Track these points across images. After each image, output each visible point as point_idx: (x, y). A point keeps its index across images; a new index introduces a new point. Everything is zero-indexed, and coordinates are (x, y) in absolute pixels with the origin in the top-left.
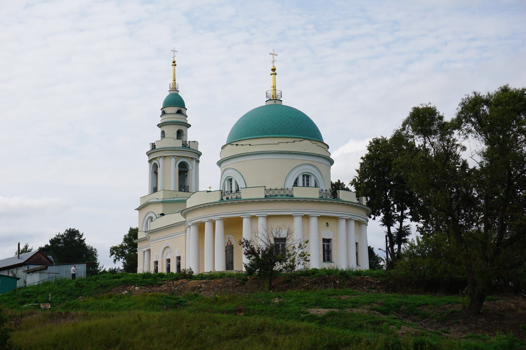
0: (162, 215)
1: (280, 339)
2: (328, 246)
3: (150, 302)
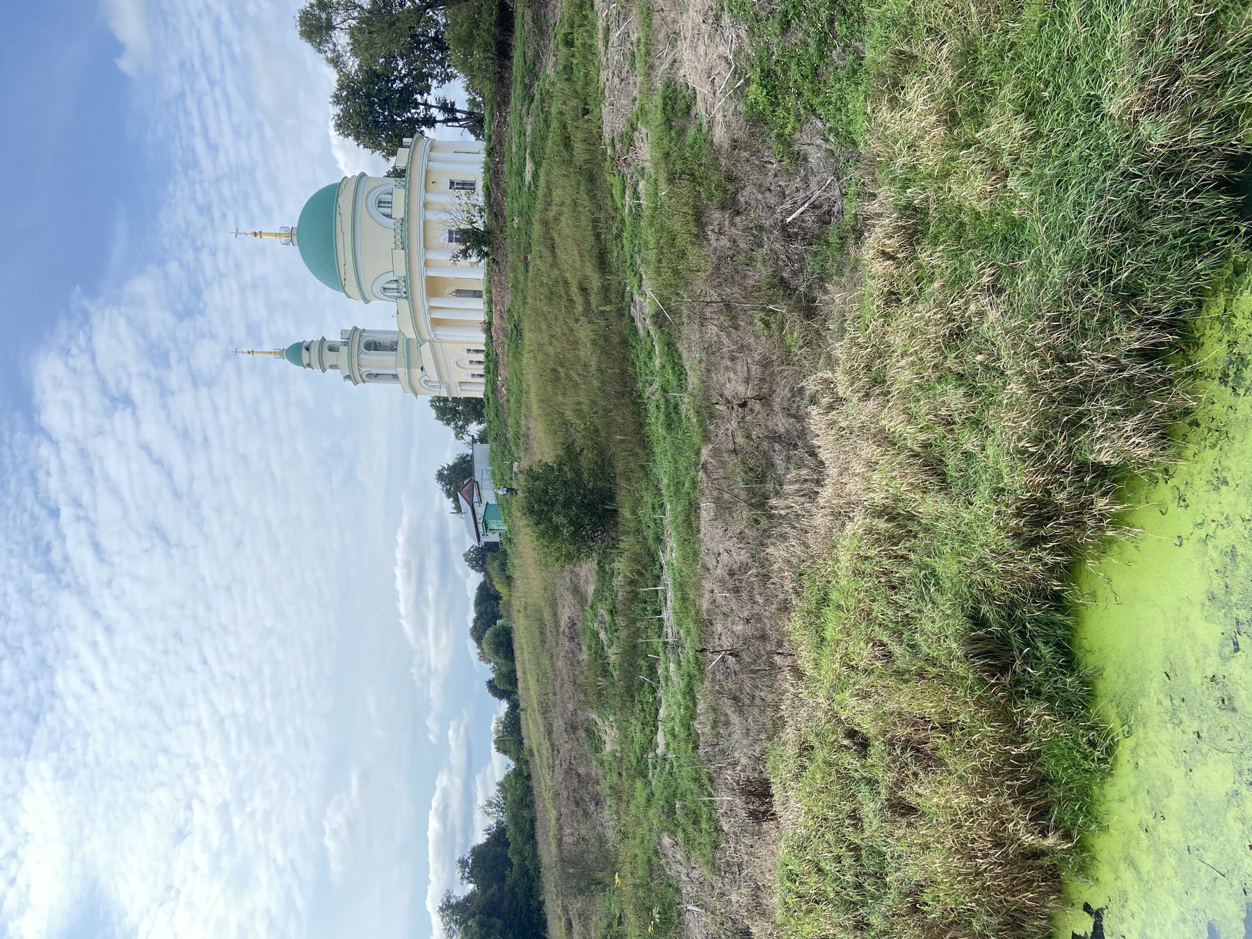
0: (422, 369)
1: (557, 200)
3: (514, 356)
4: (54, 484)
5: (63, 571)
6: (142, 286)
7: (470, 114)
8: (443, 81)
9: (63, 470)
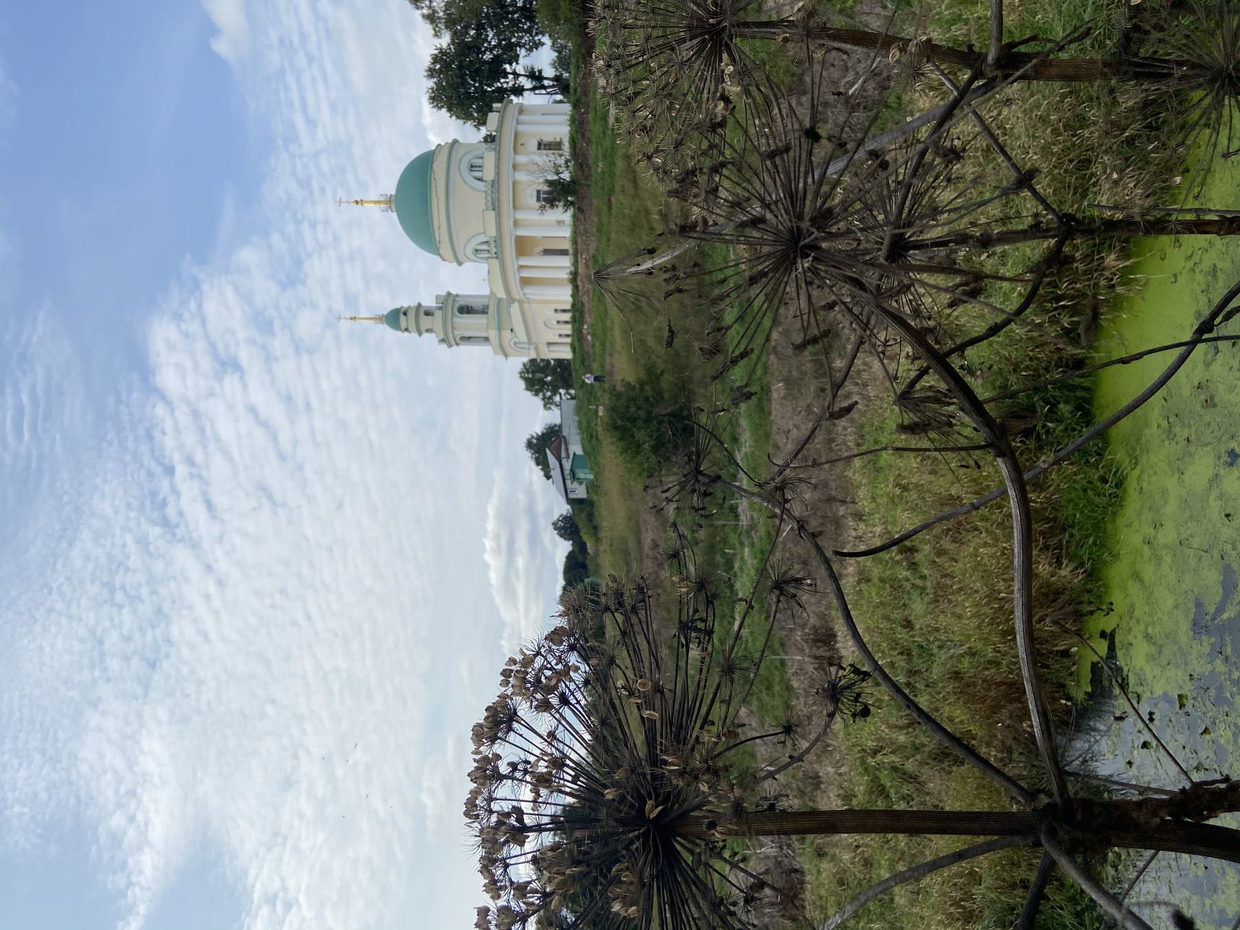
2: (545, 145)
4: (169, 442)
5: (178, 525)
6: (248, 256)
7: (557, 79)
8: (530, 50)
9: (177, 430)
